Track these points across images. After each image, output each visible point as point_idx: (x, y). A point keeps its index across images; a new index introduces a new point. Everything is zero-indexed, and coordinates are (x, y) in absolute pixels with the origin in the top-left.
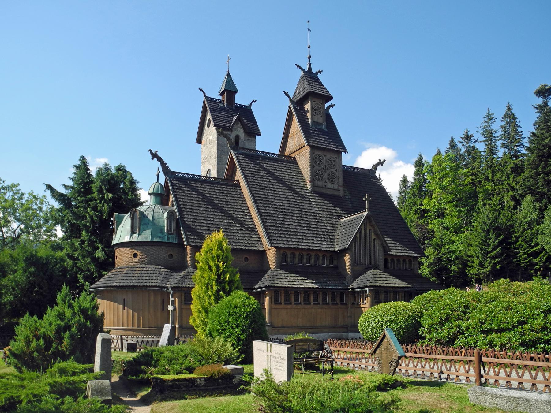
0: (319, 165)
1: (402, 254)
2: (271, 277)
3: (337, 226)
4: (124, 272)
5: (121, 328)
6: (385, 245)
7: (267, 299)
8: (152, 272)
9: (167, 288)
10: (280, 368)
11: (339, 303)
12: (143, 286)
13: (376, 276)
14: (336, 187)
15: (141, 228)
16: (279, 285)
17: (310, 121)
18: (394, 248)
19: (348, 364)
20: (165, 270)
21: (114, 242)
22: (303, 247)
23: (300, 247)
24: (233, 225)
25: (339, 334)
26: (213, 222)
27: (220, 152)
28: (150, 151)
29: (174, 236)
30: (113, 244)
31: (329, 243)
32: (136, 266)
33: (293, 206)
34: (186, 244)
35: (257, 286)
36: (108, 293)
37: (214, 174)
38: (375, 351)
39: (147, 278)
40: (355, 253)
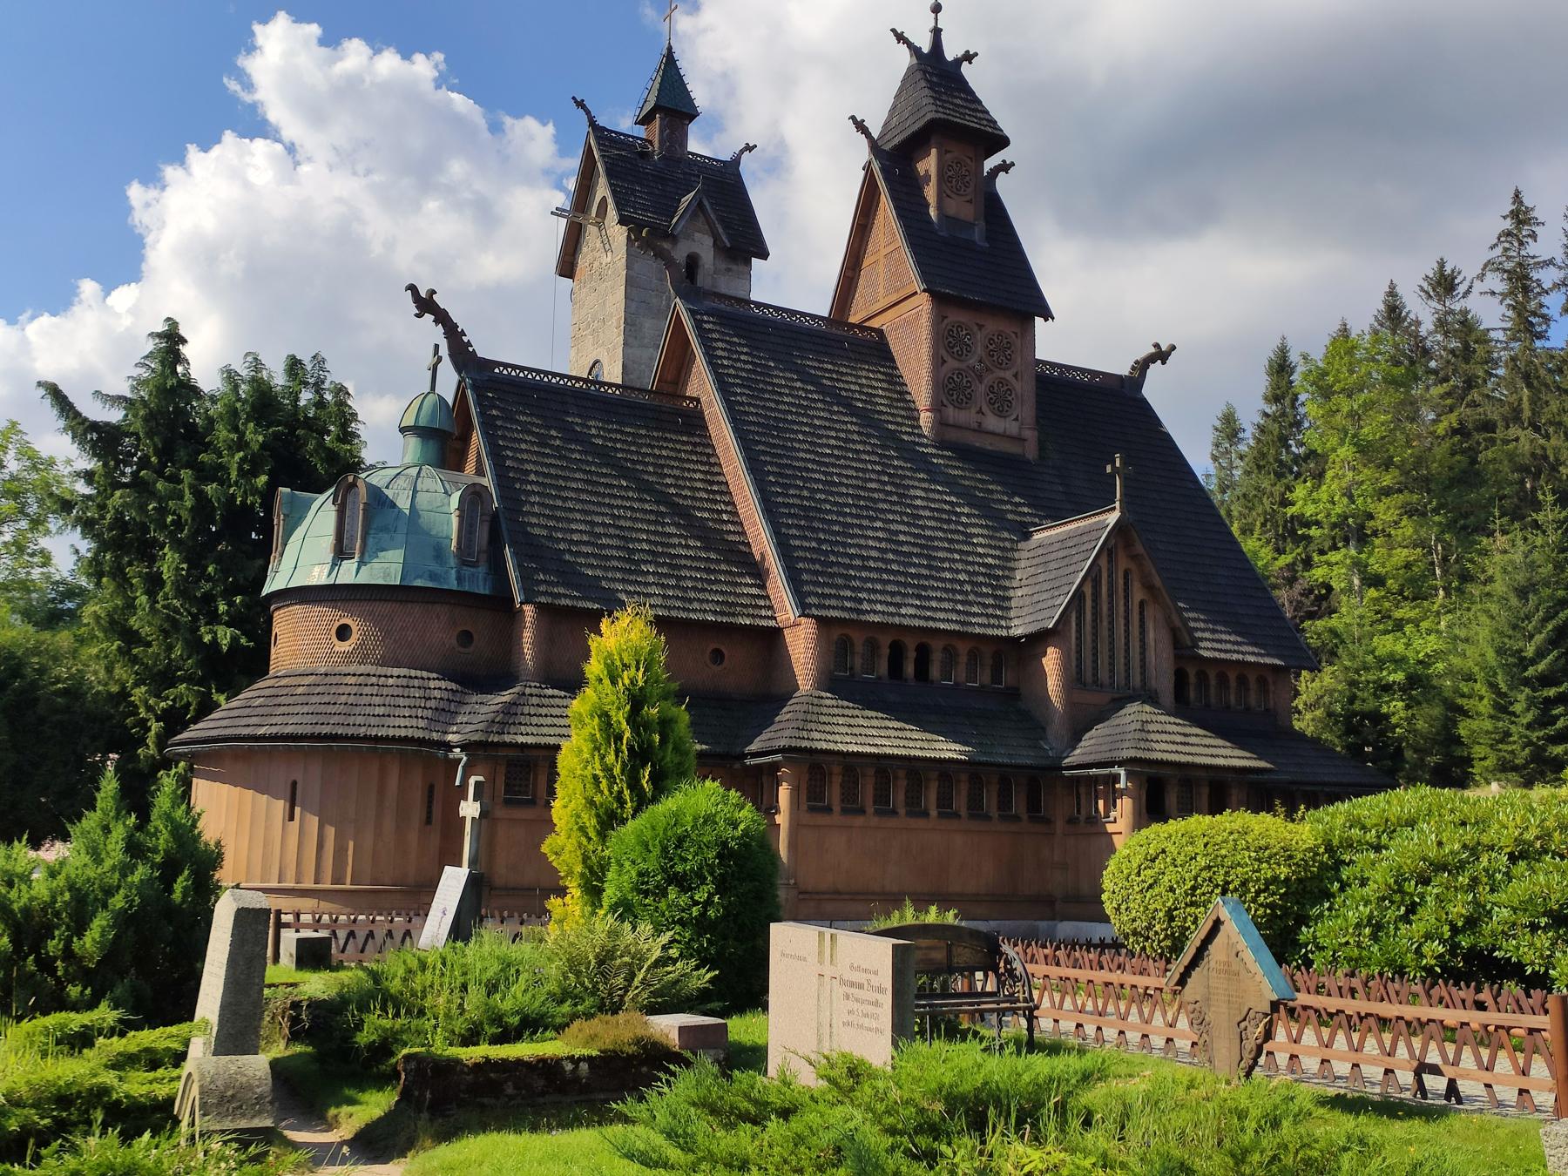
0: (959, 357)
1: (1235, 657)
2: (802, 716)
3: (1016, 555)
4: (300, 690)
5: (274, 885)
6: (1178, 623)
7: (784, 793)
8: (399, 691)
9: (449, 746)
10: (866, 1022)
11: (1025, 817)
12: (366, 738)
13: (1151, 727)
14: (1012, 427)
15: (371, 541)
16: (824, 746)
17: (933, 212)
18: (1207, 635)
19: (1079, 1026)
20: (443, 684)
21: (272, 585)
22: (906, 622)
23: (897, 620)
24: (676, 541)
25: (1024, 924)
26: (612, 531)
27: (634, 305)
28: (412, 288)
29: (482, 570)
30: (265, 592)
31: (990, 611)
32: (345, 670)
33: (873, 485)
34: (518, 598)
35: (753, 747)
36: (244, 759)
37: (613, 373)
38: (1182, 981)
39: (381, 711)
40: (1079, 645)
